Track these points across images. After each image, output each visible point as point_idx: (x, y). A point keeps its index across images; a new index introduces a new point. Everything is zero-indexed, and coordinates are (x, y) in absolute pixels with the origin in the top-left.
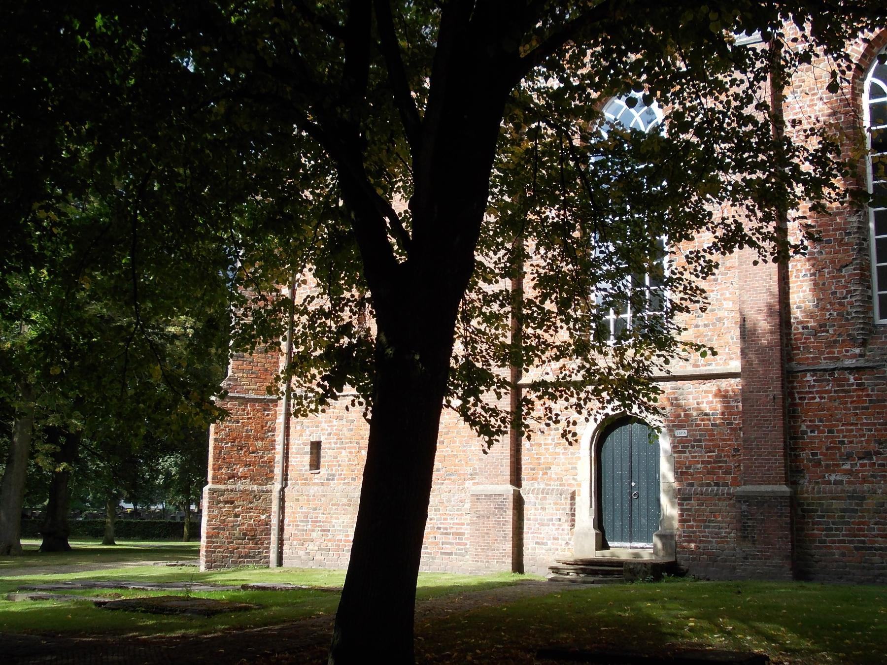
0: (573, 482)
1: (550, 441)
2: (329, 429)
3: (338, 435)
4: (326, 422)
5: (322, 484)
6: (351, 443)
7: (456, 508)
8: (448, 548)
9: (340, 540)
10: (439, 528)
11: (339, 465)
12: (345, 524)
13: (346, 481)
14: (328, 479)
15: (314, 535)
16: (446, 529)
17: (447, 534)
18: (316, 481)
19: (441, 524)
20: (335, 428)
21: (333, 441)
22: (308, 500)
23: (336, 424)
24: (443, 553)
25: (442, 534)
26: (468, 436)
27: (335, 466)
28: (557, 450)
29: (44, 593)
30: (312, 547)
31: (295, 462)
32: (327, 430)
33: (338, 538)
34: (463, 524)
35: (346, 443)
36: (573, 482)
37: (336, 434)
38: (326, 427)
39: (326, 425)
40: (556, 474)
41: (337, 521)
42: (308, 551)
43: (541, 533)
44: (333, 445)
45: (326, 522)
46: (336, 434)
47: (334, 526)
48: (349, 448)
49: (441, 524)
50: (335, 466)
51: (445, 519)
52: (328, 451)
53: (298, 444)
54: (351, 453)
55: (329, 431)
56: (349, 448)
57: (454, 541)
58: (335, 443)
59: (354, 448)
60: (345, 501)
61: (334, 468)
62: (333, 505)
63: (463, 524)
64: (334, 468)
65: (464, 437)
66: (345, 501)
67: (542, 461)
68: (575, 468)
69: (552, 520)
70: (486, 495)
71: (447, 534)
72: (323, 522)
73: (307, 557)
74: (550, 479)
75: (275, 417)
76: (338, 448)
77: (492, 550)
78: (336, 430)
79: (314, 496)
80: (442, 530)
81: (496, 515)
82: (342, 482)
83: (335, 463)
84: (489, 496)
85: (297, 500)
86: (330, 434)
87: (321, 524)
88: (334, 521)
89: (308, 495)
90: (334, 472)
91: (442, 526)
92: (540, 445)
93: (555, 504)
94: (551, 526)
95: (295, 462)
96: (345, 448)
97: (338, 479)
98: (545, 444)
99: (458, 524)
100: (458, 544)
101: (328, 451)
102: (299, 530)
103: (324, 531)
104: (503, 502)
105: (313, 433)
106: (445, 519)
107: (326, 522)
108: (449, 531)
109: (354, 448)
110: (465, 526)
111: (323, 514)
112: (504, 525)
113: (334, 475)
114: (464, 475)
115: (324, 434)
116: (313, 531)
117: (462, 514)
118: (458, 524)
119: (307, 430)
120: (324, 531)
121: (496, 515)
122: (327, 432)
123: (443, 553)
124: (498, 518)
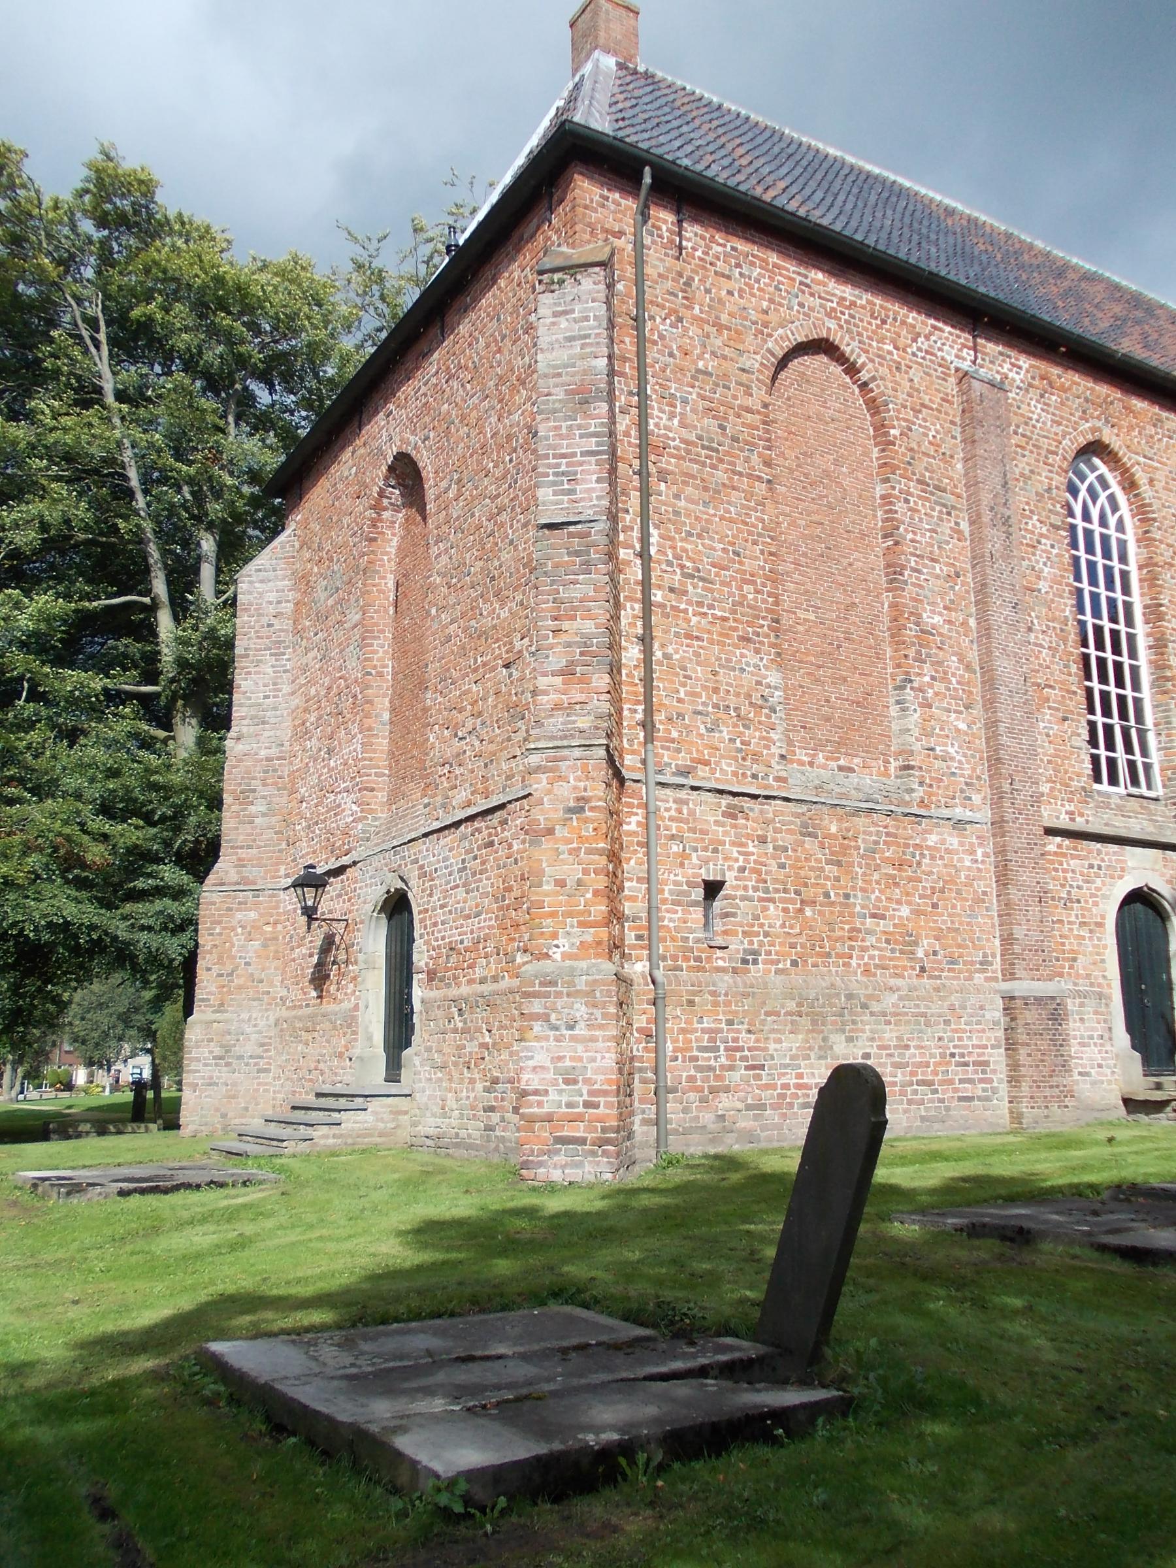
0: (1101, 980)
1: (1073, 919)
2: (741, 858)
3: (759, 872)
4: (733, 844)
5: (735, 971)
6: (785, 891)
7: (974, 1019)
8: (968, 1090)
9: (786, 1086)
10: (953, 1055)
11: (766, 934)
12: (794, 1051)
13: (780, 966)
14: (745, 961)
15: (736, 1077)
16: (962, 1055)
17: (966, 1064)
18: (721, 963)
19: (955, 1047)
20: (752, 858)
21: (750, 884)
22: (716, 1004)
23: (755, 850)
24: (961, 1099)
25: (958, 1064)
26: (972, 899)
27: (758, 934)
28: (1082, 933)
29: (631, 612)
30: (725, 1102)
31: (671, 920)
32: (737, 860)
33: (784, 1080)
34: (985, 1047)
35: (777, 891)
36: (1101, 980)
37: (753, 871)
38: (736, 855)
39: (735, 849)
40: (1084, 968)
41: (778, 1046)
42: (720, 1113)
43: (1082, 1058)
44: (751, 892)
45: (756, 1049)
46: (753, 871)
47: (772, 1058)
48: (783, 900)
49: (955, 1047)
50: (758, 934)
51: (960, 1039)
52: (741, 904)
53: (676, 883)
54: (786, 910)
55: (741, 863)
56: (783, 900)
57: (976, 1076)
58: (756, 889)
59: (792, 901)
60: (792, 1005)
61: (755, 940)
62: (768, 1014)
63: (985, 1047)
64: (755, 940)
65: (967, 900)
66: (792, 1005)
67: (1067, 947)
68: (1103, 961)
69: (1091, 1038)
70: (1036, 998)
71: (966, 1064)
72: (749, 1049)
73: (721, 1125)
74: (1078, 976)
75: (1137, 554)
76: (761, 900)
77: (1051, 1087)
78: (755, 862)
79: (726, 995)
80: (957, 1058)
81: (1050, 1030)
82: (773, 968)
83: (756, 929)
84: (1039, 1000)
85: (691, 1003)
86: (742, 870)
87: (746, 1053)
88: (772, 1046)
89: (714, 994)
90: (756, 946)
91: (956, 1051)
92: (1061, 922)
93: (1096, 1013)
94: (1092, 1047)
95: (671, 920)
96: (772, 900)
97: (765, 962)
98: (1069, 923)
99: (979, 1047)
100: (981, 1081)
101: (741, 904)
102: (699, 1069)
103: (753, 1067)
104: (1056, 1009)
105: (707, 863)
106: (960, 1039)
107: (756, 1049)
108: (967, 1059)
109: (792, 901)
110: (989, 1050)
111: (749, 1032)
112: (1061, 1045)
113: (755, 953)
114: (972, 963)
115: (730, 868)
116: (731, 1068)
117: (983, 1031)
118: (979, 1047)
119: (694, 855)
120: (753, 1067)
121: (1050, 1030)
122: (736, 865)
123: (961, 1099)
124: (1054, 1035)
